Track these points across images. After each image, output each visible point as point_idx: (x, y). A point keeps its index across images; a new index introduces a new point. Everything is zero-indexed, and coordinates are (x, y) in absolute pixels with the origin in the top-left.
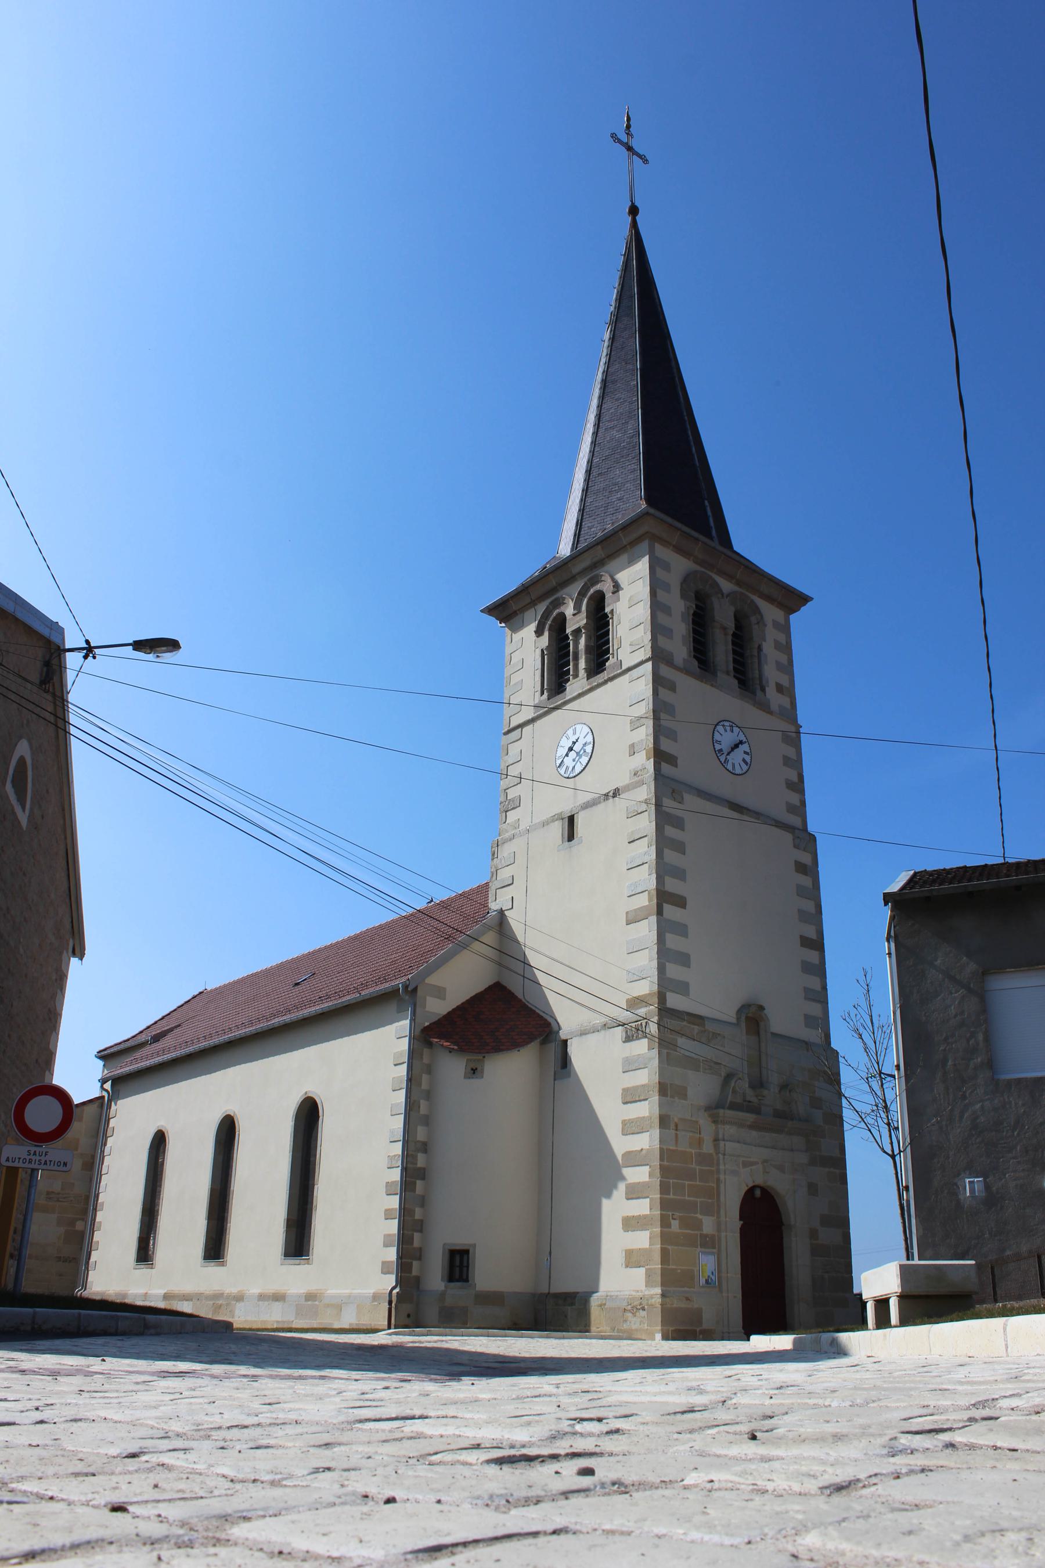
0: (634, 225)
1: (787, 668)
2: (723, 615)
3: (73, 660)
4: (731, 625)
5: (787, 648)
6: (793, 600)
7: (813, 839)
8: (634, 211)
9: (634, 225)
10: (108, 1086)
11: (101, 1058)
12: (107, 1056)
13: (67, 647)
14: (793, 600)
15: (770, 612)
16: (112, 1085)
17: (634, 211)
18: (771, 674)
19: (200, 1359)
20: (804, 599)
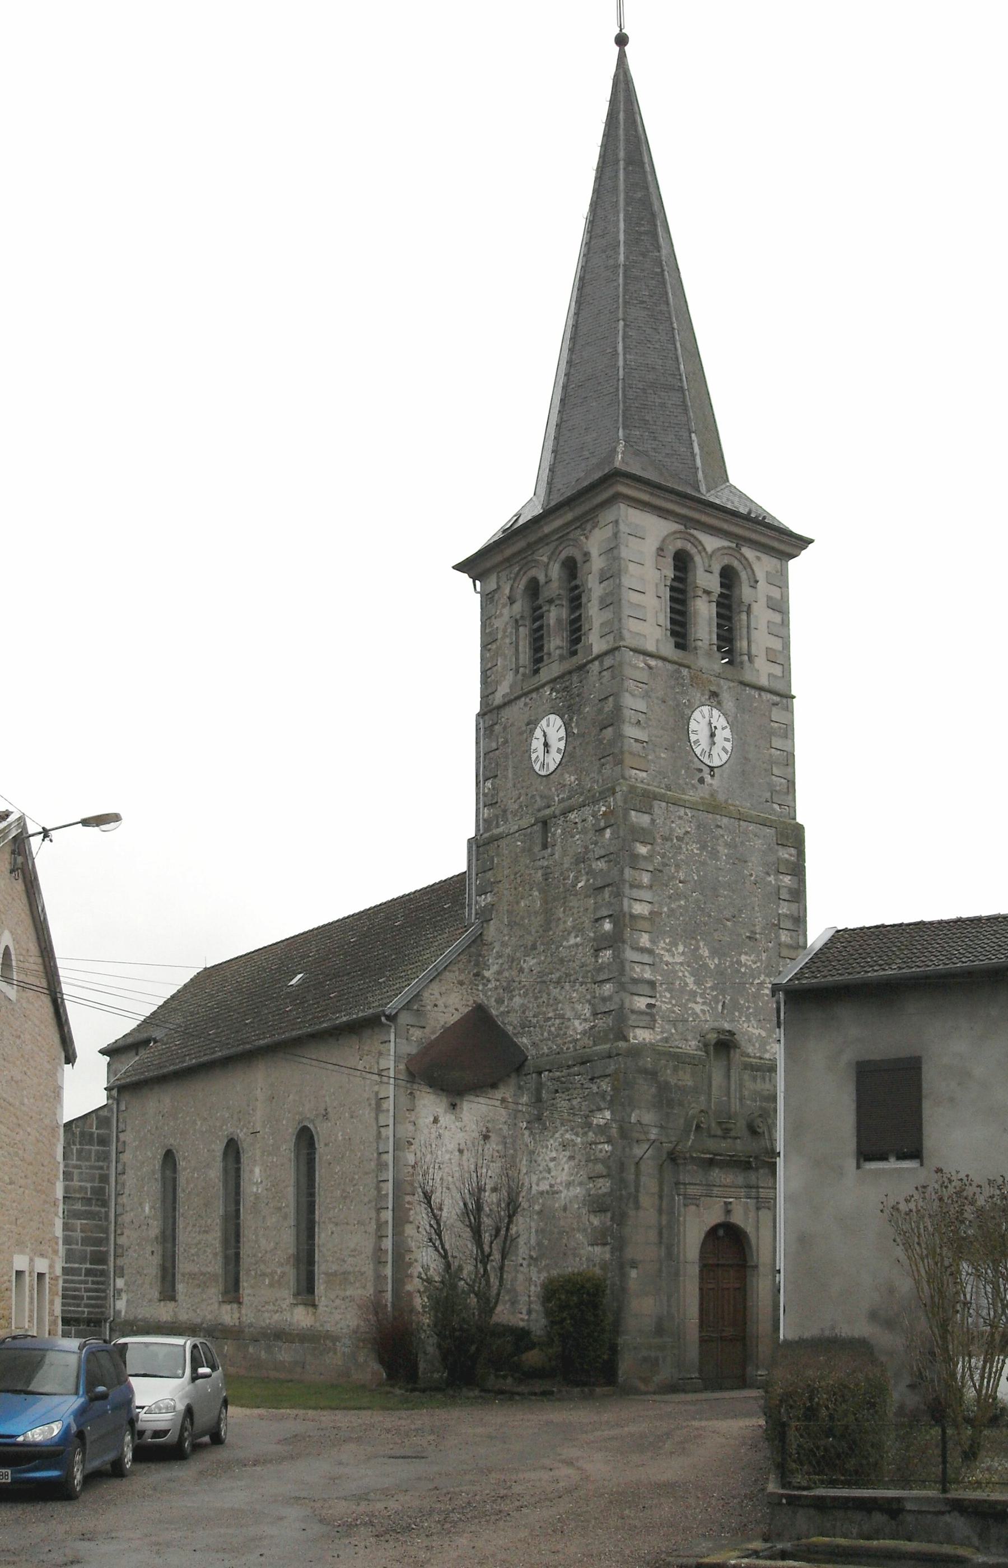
0: (622, 58)
1: (781, 630)
2: (706, 580)
3: (35, 842)
4: (716, 588)
5: (780, 607)
6: (788, 544)
7: (799, 829)
8: (622, 40)
9: (622, 58)
10: (115, 1092)
11: (103, 1052)
12: (111, 1052)
13: (30, 832)
14: (788, 544)
15: (762, 565)
16: (118, 1092)
17: (622, 40)
18: (761, 640)
19: (713, 429)
20: (804, 542)
